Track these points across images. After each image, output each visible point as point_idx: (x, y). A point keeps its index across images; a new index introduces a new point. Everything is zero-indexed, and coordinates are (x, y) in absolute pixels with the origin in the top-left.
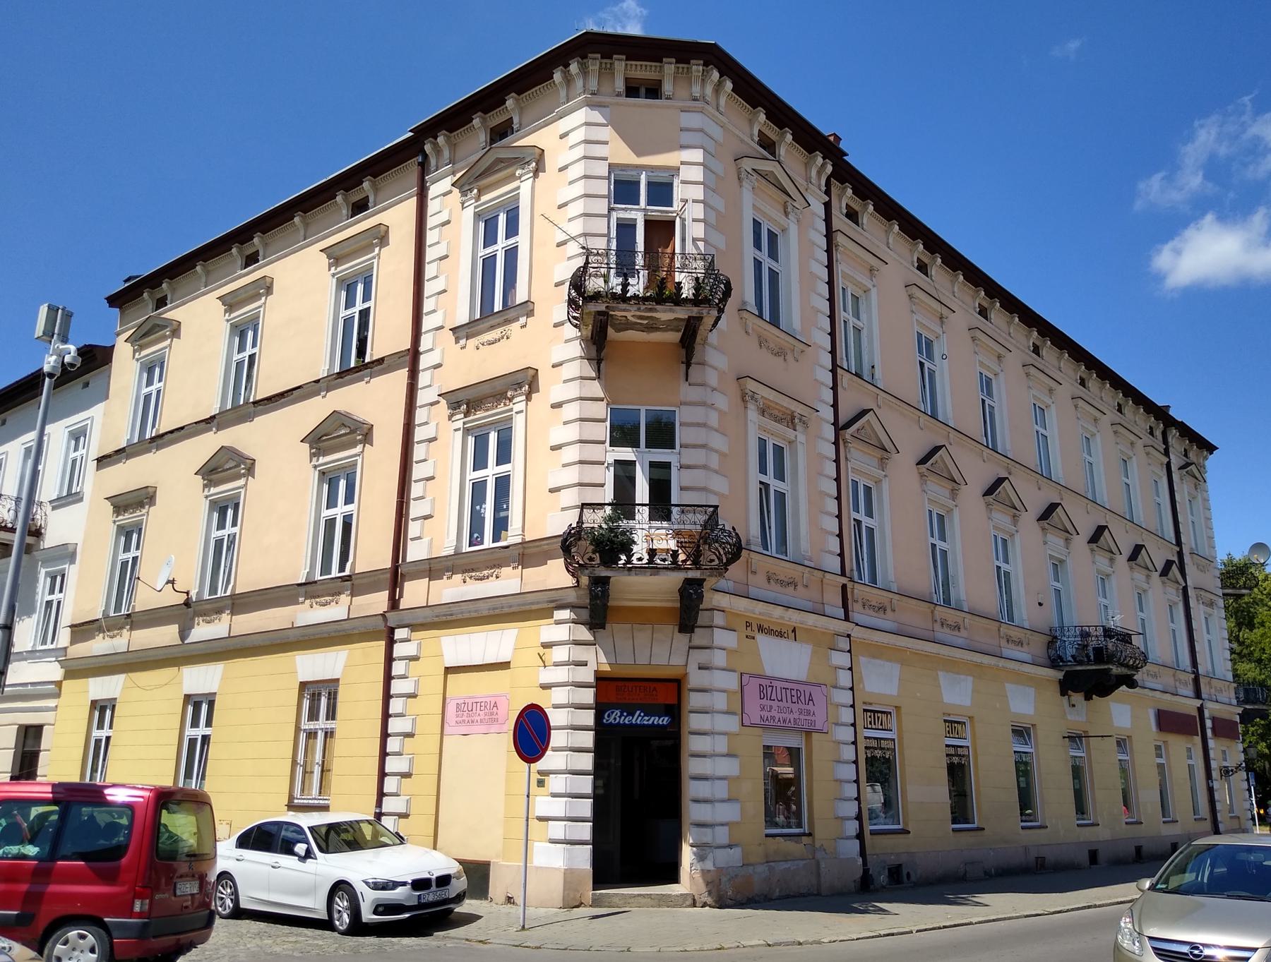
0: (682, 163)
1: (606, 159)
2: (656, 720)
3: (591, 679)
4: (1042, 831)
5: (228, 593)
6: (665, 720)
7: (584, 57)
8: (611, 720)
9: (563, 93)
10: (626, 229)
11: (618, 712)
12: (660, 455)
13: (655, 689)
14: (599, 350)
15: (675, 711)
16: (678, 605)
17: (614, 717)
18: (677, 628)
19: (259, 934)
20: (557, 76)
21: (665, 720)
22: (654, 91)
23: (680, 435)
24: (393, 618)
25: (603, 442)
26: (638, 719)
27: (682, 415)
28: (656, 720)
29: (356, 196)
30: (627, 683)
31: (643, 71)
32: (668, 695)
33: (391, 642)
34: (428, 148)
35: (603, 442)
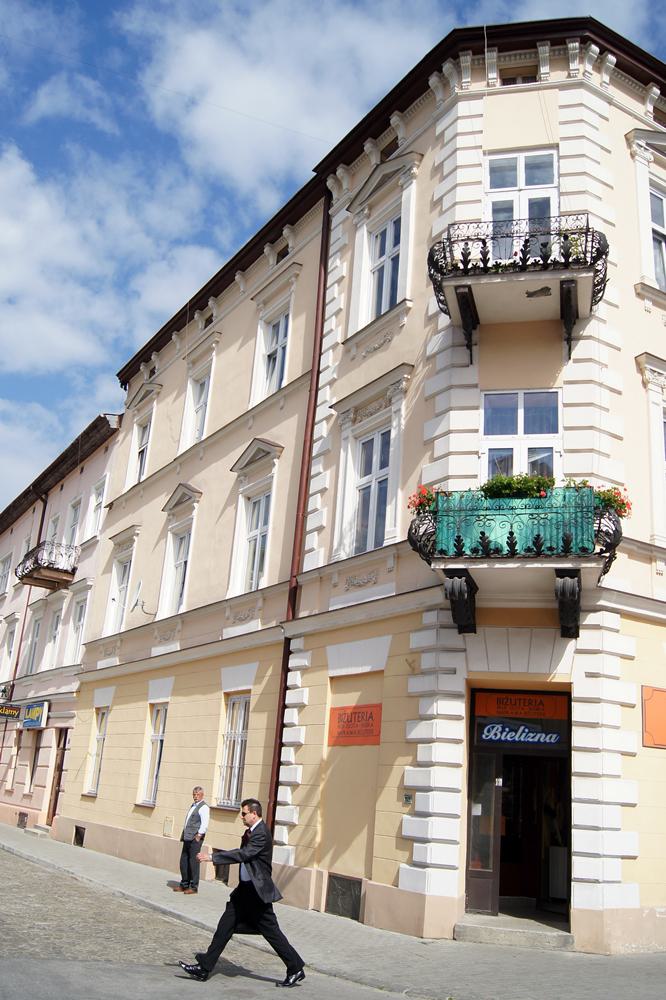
0: (563, 139)
1: (481, 147)
2: (542, 737)
3: (462, 688)
4: (188, 563)
5: (539, 735)
6: (552, 738)
7: (456, 57)
8: (492, 736)
9: (439, 96)
10: (503, 210)
11: (499, 727)
12: (541, 440)
13: (541, 702)
14: (468, 336)
15: (565, 726)
16: (556, 605)
17: (494, 733)
18: (559, 633)
19: (505, 925)
20: (433, 81)
21: (552, 738)
22: (531, 76)
23: (565, 417)
24: (291, 629)
25: (476, 431)
26: (522, 735)
27: (565, 395)
28: (542, 737)
29: (280, 246)
30: (510, 696)
31: (517, 60)
32: (553, 706)
33: (287, 653)
34: (330, 183)
35: (476, 431)
